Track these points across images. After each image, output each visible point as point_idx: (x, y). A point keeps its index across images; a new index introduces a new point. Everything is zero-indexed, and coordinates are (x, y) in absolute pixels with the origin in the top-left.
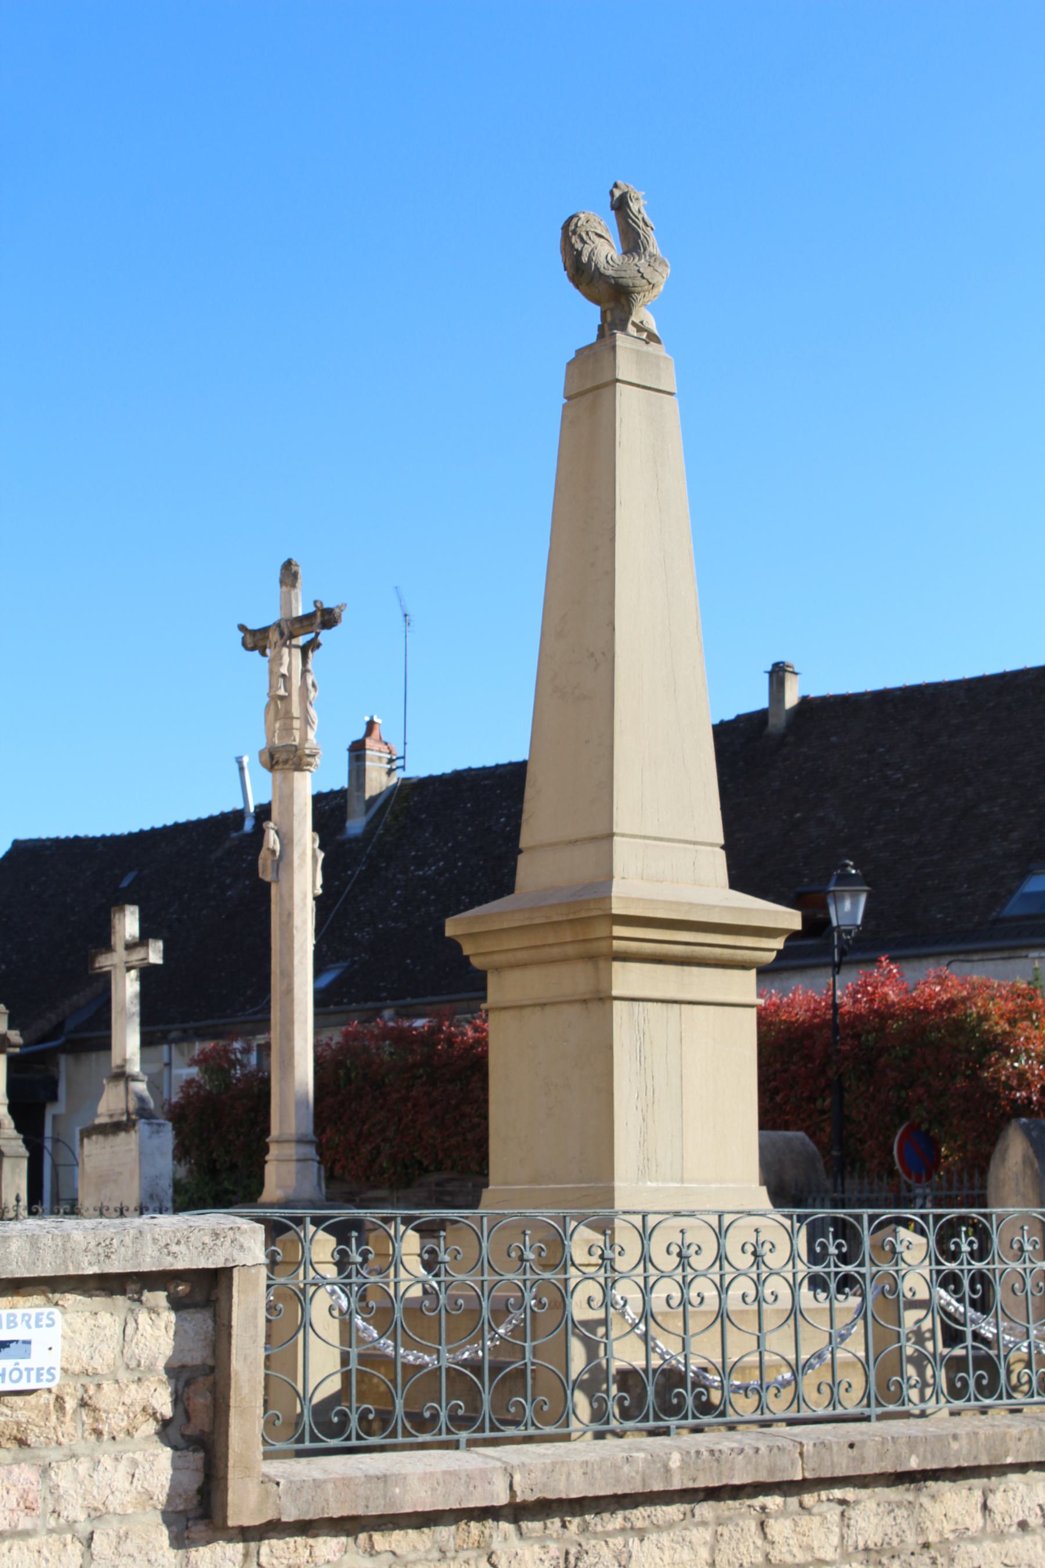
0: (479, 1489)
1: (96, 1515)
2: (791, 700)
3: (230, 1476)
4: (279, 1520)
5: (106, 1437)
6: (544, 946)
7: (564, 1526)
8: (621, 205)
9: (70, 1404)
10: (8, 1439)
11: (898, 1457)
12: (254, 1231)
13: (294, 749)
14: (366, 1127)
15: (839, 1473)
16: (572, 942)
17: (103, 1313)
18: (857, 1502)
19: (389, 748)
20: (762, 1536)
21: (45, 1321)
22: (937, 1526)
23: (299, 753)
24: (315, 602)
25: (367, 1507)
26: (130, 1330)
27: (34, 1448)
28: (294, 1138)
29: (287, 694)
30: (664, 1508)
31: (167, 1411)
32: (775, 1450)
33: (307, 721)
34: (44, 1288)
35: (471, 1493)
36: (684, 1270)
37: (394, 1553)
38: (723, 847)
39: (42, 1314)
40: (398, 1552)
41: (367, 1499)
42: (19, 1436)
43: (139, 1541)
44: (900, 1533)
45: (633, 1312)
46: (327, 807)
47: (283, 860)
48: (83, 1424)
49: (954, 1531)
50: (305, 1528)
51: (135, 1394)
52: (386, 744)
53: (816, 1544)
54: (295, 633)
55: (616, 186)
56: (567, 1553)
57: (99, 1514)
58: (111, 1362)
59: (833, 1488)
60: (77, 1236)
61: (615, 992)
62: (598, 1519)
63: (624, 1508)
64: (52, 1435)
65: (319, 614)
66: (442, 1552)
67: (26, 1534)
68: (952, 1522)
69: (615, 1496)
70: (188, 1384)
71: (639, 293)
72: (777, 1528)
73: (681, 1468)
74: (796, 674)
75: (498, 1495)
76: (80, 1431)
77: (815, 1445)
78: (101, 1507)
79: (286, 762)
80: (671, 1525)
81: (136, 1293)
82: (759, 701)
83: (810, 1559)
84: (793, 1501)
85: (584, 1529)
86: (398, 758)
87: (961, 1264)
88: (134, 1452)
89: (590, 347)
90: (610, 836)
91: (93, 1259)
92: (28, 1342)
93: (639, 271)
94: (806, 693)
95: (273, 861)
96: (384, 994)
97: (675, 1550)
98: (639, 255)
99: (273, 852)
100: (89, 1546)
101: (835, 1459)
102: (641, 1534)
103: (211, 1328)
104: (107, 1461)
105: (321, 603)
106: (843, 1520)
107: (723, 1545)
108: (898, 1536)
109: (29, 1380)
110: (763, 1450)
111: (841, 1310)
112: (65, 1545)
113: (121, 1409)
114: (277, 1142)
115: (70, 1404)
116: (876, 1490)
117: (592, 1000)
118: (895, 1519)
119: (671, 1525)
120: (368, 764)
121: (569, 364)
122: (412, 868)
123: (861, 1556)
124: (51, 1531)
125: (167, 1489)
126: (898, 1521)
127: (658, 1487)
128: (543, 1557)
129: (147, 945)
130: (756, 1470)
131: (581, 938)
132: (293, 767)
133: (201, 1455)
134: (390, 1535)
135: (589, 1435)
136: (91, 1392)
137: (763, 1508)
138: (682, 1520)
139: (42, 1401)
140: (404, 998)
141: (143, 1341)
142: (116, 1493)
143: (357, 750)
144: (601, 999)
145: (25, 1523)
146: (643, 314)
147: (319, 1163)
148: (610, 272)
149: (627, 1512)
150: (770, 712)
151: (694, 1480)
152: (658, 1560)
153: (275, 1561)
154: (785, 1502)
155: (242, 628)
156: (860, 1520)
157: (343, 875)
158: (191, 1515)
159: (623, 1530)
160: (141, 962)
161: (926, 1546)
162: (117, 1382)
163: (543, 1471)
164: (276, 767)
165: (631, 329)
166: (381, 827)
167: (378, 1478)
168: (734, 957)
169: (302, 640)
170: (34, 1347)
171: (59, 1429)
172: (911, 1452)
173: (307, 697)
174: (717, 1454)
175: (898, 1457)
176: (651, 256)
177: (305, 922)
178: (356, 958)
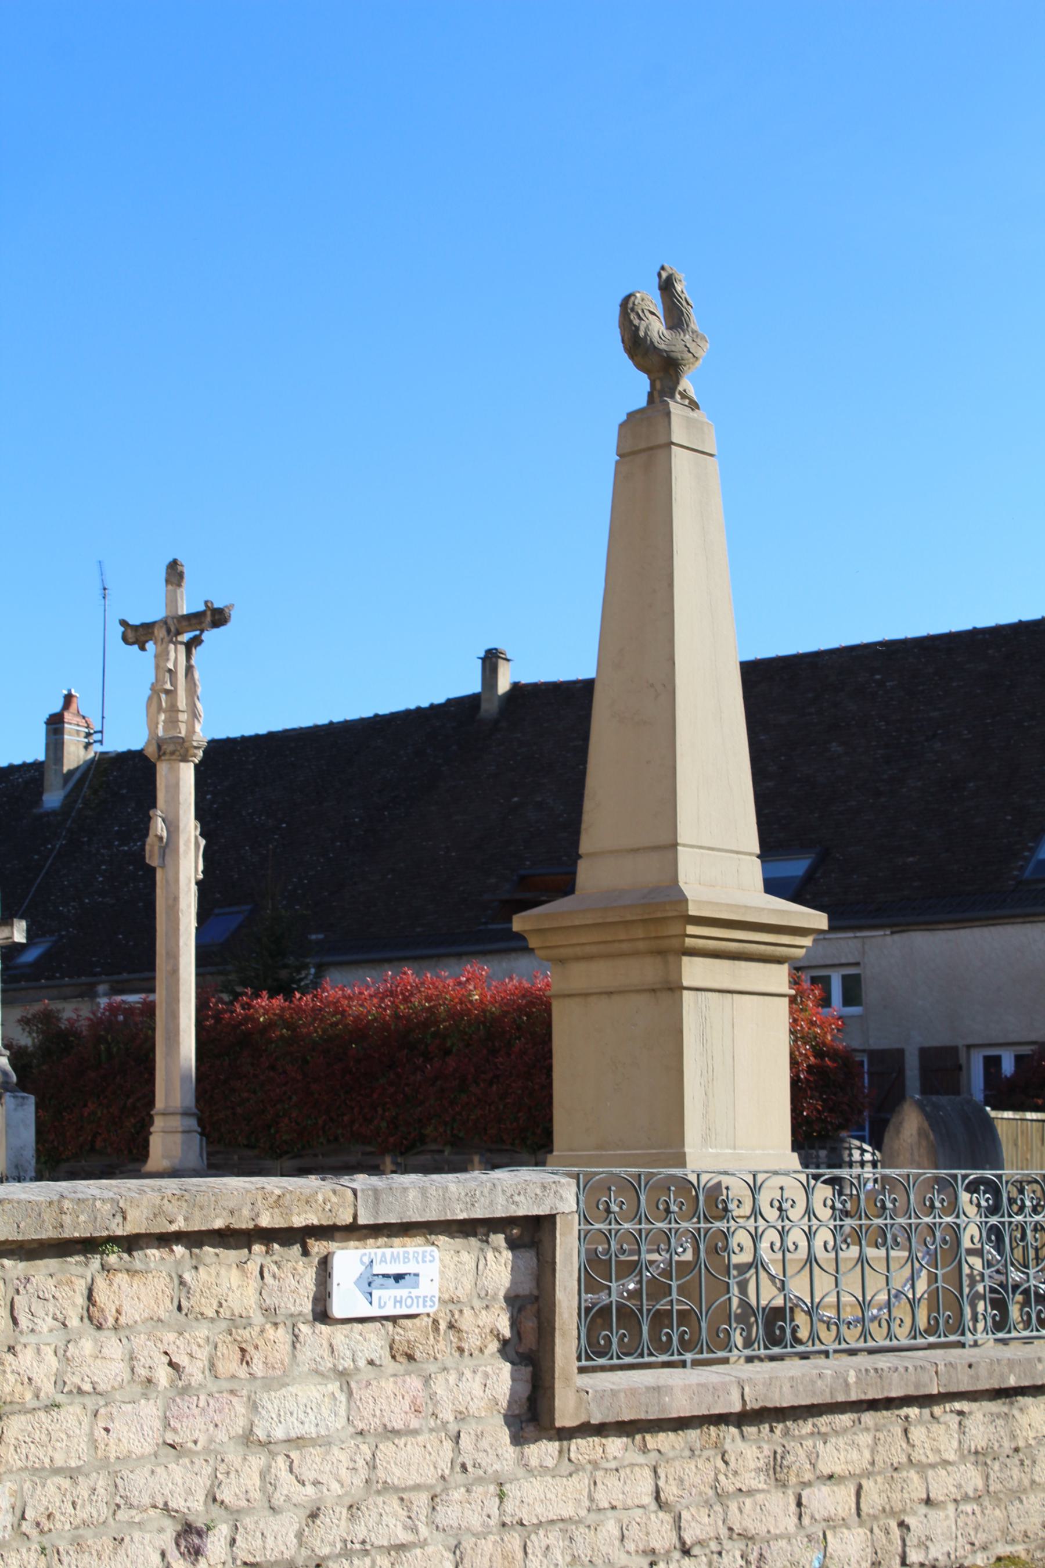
0: (722, 1398)
1: (461, 1416)
2: (503, 686)
3: (557, 1386)
4: (589, 1422)
5: (466, 1353)
6: (614, 941)
7: (772, 1430)
8: (667, 286)
9: (443, 1326)
10: (401, 1355)
11: (1002, 1376)
12: (569, 1184)
13: (181, 741)
14: (130, 1101)
15: (963, 1388)
16: (643, 939)
17: (462, 1251)
18: (970, 1413)
19: (86, 722)
20: (906, 1440)
21: (429, 1258)
22: (1024, 1434)
23: (186, 744)
24: (206, 602)
25: (647, 1412)
26: (481, 1267)
27: (420, 1362)
28: (180, 1110)
29: (172, 688)
30: (840, 1416)
31: (507, 1332)
32: (919, 1369)
33: (194, 715)
34: (425, 1231)
35: (716, 1402)
36: (809, 1220)
37: (659, 1451)
38: (759, 857)
39: (426, 1252)
40: (662, 1450)
41: (647, 1406)
42: (409, 1352)
43: (491, 1439)
44: (1000, 1439)
45: (802, 1253)
46: (20, 780)
47: (169, 847)
48: (451, 1342)
49: (1035, 1438)
50: (601, 1430)
51: (486, 1319)
52: (84, 717)
53: (942, 1448)
54: (181, 631)
55: (663, 268)
56: (775, 1453)
57: (463, 1416)
58: (469, 1292)
59: (954, 1401)
60: (453, 1187)
61: (685, 983)
62: (795, 1425)
63: (813, 1416)
64: (431, 1352)
65: (209, 613)
66: (692, 1450)
67: (415, 1432)
68: (1034, 1431)
69: (813, 1406)
70: (520, 1310)
71: (685, 366)
72: (917, 1434)
73: (856, 1383)
74: (508, 660)
75: (734, 1404)
76: (449, 1349)
77: (945, 1365)
78: (464, 1410)
79: (172, 753)
80: (845, 1430)
81: (484, 1235)
82: (472, 684)
83: (938, 1460)
84: (926, 1412)
85: (786, 1433)
86: (96, 732)
87: (934, 1218)
88: (486, 1366)
89: (641, 411)
90: (674, 846)
91: (463, 1206)
92: (417, 1275)
93: (686, 346)
94: (517, 680)
95: (160, 847)
96: (98, 969)
97: (847, 1451)
98: (683, 331)
99: (161, 838)
100: (458, 1443)
101: (960, 1376)
102: (824, 1438)
103: (535, 1266)
104: (468, 1374)
105: (212, 603)
106: (960, 1428)
107: (880, 1448)
108: (998, 1441)
109: (418, 1306)
110: (911, 1369)
111: (792, 1260)
112: (441, 1442)
113: (477, 1331)
114: (164, 1114)
115: (443, 1326)
116: (983, 1403)
117: (661, 990)
118: (996, 1427)
119: (845, 1430)
120: (66, 737)
121: (622, 426)
122: (116, 843)
123: (972, 1458)
124: (431, 1430)
125: (508, 1397)
126: (998, 1429)
127: (841, 1398)
128: (759, 1456)
129: (12, 925)
130: (907, 1385)
131: (653, 935)
132: (180, 758)
133: (530, 1369)
134: (657, 1436)
135: (742, 1360)
136: (456, 1316)
137: (907, 1417)
138: (852, 1427)
139: (424, 1323)
140: (120, 973)
141: (490, 1274)
142: (475, 1399)
143: (55, 724)
144: (671, 989)
145: (415, 1424)
146: (686, 384)
147: (202, 1134)
148: (662, 346)
149: (815, 1420)
150: (483, 697)
151: (865, 1393)
152: (836, 1459)
153: (580, 1457)
154: (921, 1413)
155: (123, 623)
156: (972, 1428)
157: (42, 848)
158: (524, 1418)
159: (812, 1434)
160: (5, 941)
161: (1017, 1450)
162: (473, 1308)
163: (764, 1384)
164: (163, 758)
165: (678, 397)
166: (80, 801)
167: (654, 1389)
168: (746, 950)
169: (185, 637)
170: (421, 1279)
171: (436, 1347)
172: (1011, 1372)
173: (195, 692)
174: (880, 1371)
175: (1002, 1376)
176: (694, 332)
177: (189, 906)
178: (63, 933)
